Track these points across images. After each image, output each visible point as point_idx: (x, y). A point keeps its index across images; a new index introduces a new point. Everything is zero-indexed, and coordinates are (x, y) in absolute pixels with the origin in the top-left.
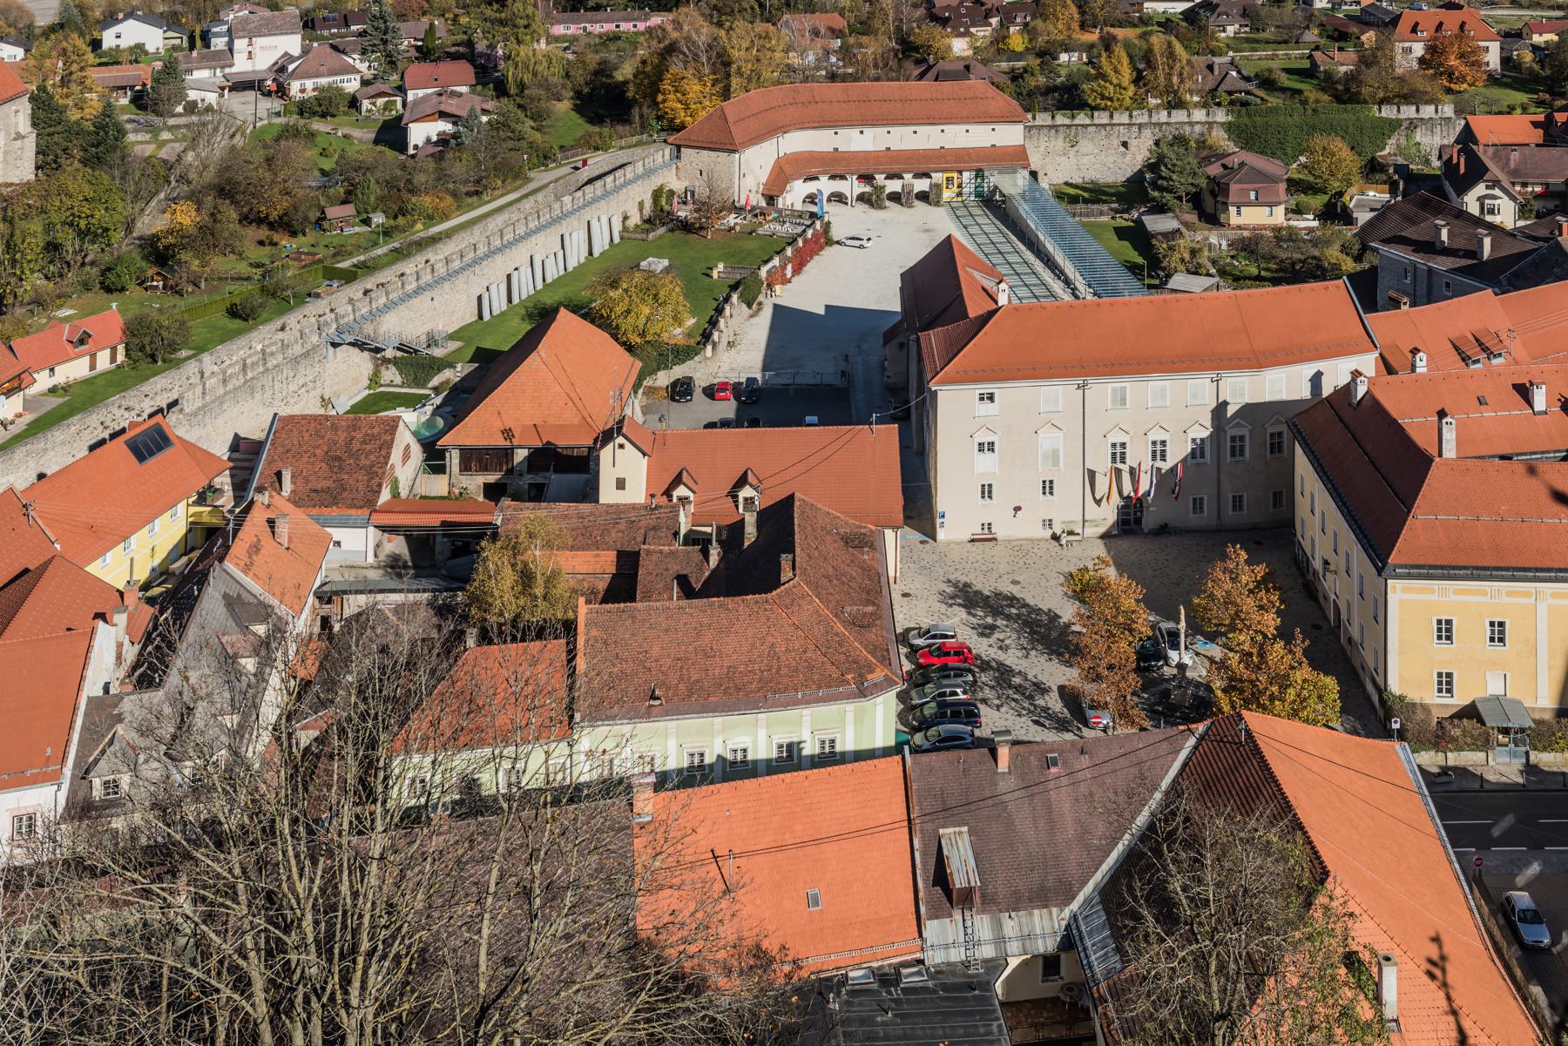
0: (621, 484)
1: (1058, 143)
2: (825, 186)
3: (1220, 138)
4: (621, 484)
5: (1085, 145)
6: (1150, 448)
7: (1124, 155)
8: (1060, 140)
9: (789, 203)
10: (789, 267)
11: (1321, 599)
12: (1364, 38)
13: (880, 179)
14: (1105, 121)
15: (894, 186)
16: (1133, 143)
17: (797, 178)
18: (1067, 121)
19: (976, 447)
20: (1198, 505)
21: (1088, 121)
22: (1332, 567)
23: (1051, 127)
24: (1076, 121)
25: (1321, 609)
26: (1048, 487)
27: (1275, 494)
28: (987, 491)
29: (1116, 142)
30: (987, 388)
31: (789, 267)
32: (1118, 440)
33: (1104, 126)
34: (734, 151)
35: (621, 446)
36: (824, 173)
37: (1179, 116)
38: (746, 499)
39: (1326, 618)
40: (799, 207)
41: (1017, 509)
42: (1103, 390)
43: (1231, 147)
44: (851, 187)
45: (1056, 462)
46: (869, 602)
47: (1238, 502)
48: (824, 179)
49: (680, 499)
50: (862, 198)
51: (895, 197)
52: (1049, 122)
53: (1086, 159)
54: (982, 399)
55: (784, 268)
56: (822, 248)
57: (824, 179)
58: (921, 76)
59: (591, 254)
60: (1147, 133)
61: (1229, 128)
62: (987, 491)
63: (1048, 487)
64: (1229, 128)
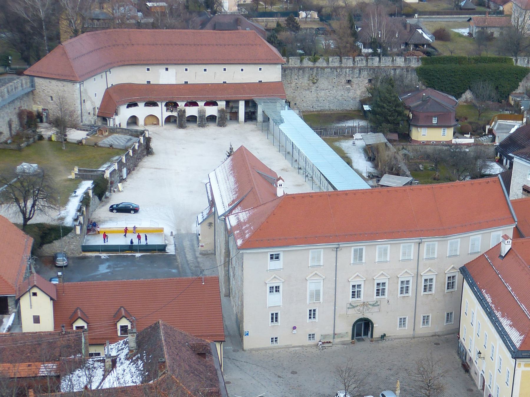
0: (37, 320)
1: (304, 81)
2: (141, 111)
3: (412, 78)
4: (37, 320)
5: (323, 83)
6: (399, 286)
7: (348, 90)
8: (306, 78)
9: (117, 123)
10: (125, 170)
11: (473, 374)
12: (97, 10)
13: (181, 105)
14: (337, 64)
15: (191, 111)
16: (355, 81)
17: (122, 105)
18: (310, 64)
19: (268, 290)
20: (402, 321)
21: (325, 65)
22: (482, 355)
23: (299, 69)
24: (317, 64)
25: (473, 380)
26: (312, 314)
27: (448, 314)
28: (275, 318)
29: (344, 81)
30: (274, 251)
31: (125, 170)
32: (405, 279)
33: (336, 68)
34: (74, 82)
35: (35, 294)
36: (141, 101)
37: (386, 62)
38: (122, 327)
39: (475, 385)
40: (124, 126)
41: (294, 328)
42: (348, 252)
43: (420, 85)
44: (161, 111)
45: (318, 298)
46: (212, 386)
47: (426, 320)
48: (141, 105)
49: (77, 328)
50: (169, 120)
51: (192, 119)
52: (298, 65)
53: (322, 93)
54: (272, 258)
55: (120, 170)
56: (144, 156)
57: (141, 105)
58: (203, 26)
59: (361, 139)
60: (365, 73)
61: (420, 72)
62: (275, 318)
63: (312, 314)
64: (420, 72)
